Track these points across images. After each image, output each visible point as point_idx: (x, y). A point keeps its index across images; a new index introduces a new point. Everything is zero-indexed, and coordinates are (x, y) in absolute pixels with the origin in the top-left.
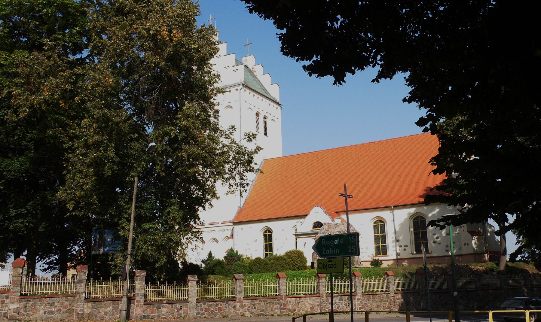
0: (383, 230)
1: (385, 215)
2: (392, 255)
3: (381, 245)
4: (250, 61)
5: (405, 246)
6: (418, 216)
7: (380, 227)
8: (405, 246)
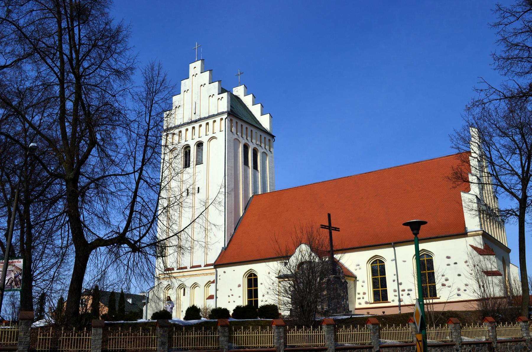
0: (383, 272)
1: (386, 253)
2: (393, 301)
3: (380, 289)
4: (239, 91)
5: (408, 290)
6: (377, 260)
7: (378, 270)
8: (408, 290)
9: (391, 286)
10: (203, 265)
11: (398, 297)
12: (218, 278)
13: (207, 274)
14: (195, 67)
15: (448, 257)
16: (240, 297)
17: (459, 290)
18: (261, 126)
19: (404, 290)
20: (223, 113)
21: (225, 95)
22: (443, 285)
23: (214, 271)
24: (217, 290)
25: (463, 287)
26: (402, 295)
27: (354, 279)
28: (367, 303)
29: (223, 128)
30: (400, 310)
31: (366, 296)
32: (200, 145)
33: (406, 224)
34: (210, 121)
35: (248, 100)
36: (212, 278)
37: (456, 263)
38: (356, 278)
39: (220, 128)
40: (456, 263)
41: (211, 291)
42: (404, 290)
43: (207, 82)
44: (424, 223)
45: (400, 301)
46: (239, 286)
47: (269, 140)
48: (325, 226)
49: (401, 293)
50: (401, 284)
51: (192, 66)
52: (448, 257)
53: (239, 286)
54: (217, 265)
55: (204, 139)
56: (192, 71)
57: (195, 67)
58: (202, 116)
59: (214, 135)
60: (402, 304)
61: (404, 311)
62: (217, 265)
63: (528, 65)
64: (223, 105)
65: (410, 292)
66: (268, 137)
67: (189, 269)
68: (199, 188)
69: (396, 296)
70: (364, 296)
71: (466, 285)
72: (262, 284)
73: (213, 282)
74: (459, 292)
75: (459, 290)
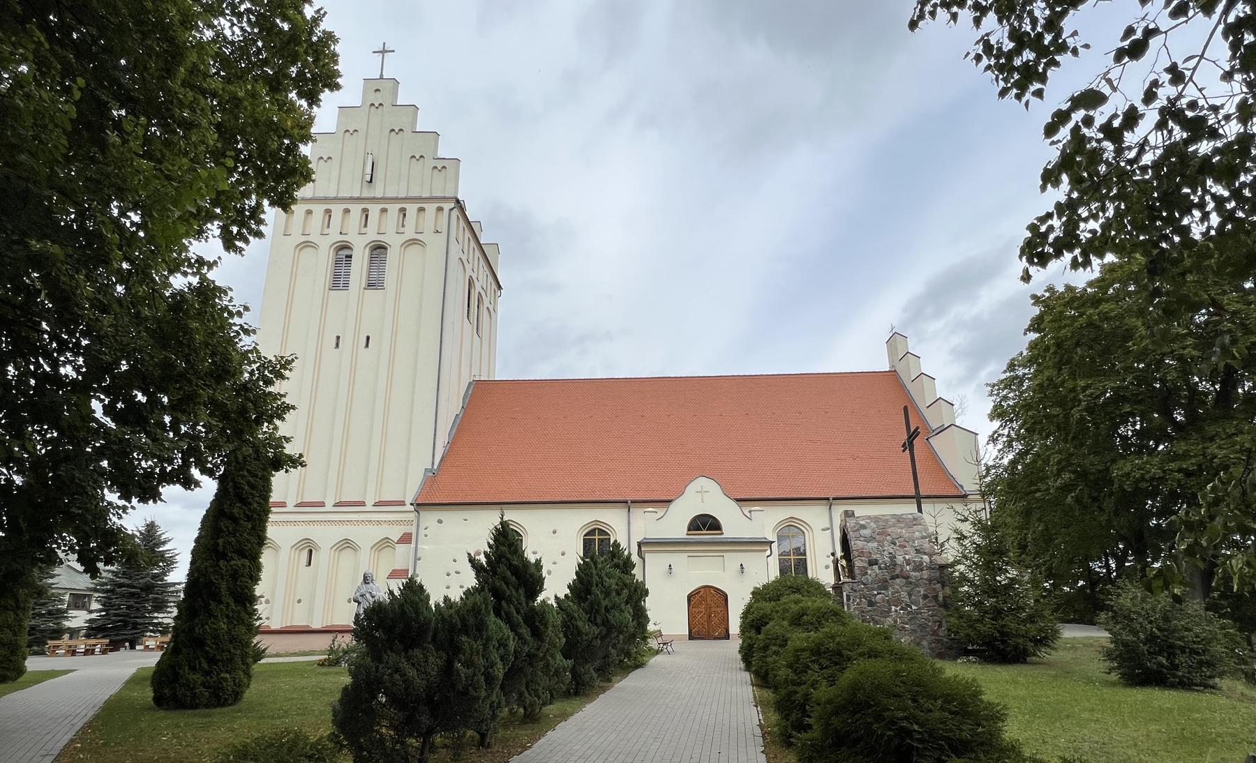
10: (370, 502)
32: (379, 249)
54: (420, 506)
55: (393, 241)
63: (695, 760)
67: (369, 507)
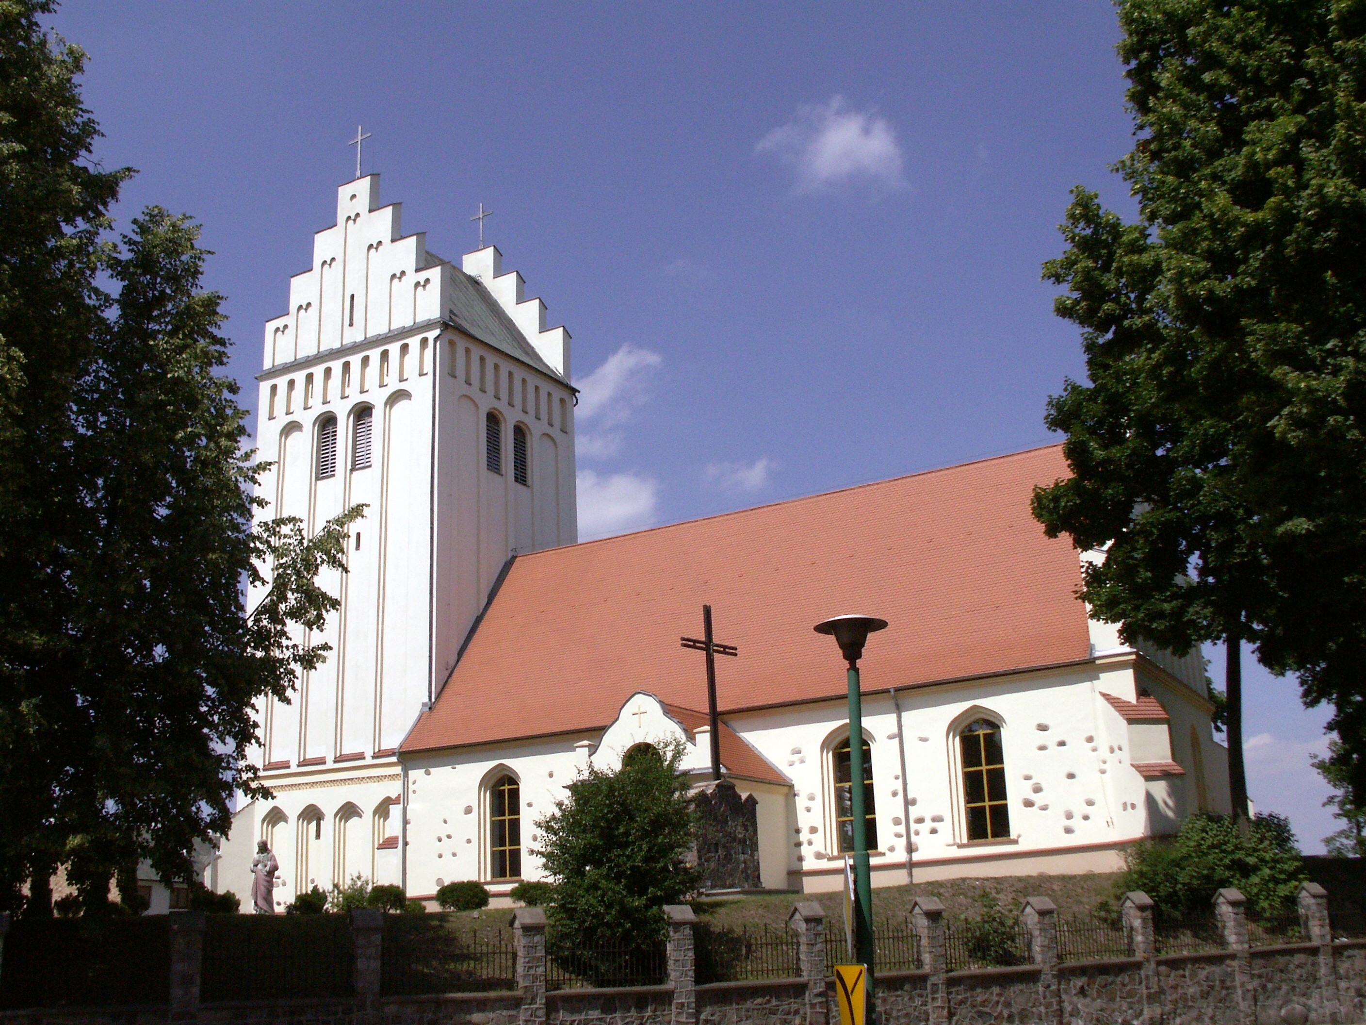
2: (892, 849)
4: (479, 263)
7: (851, 760)
9: (886, 809)
10: (369, 754)
11: (905, 838)
12: (412, 787)
13: (379, 778)
14: (355, 194)
15: (1043, 728)
16: (469, 841)
17: (1069, 816)
18: (539, 359)
19: (920, 820)
20: (428, 326)
21: (435, 274)
22: (1029, 804)
23: (398, 770)
24: (405, 822)
25: (1080, 808)
26: (917, 833)
27: (785, 789)
28: (819, 856)
29: (428, 367)
30: (911, 875)
31: (818, 838)
33: (825, 628)
34: (394, 348)
35: (503, 289)
36: (393, 789)
37: (1062, 744)
38: (791, 787)
39: (418, 371)
40: (1062, 744)
41: (393, 827)
42: (920, 820)
43: (386, 236)
44: (878, 625)
45: (911, 848)
46: (468, 810)
47: (562, 401)
48: (695, 641)
49: (913, 827)
50: (914, 802)
51: (344, 192)
52: (1043, 728)
53: (468, 810)
55: (377, 398)
56: (344, 207)
57: (355, 194)
58: (372, 332)
59: (403, 386)
60: (916, 857)
61: (922, 876)
62: (412, 756)
64: (430, 305)
65: (936, 825)
66: (558, 394)
68: (358, 535)
69: (898, 836)
70: (813, 837)
71: (1090, 803)
72: (530, 805)
73: (396, 801)
74: (1069, 823)
75: (1069, 816)
